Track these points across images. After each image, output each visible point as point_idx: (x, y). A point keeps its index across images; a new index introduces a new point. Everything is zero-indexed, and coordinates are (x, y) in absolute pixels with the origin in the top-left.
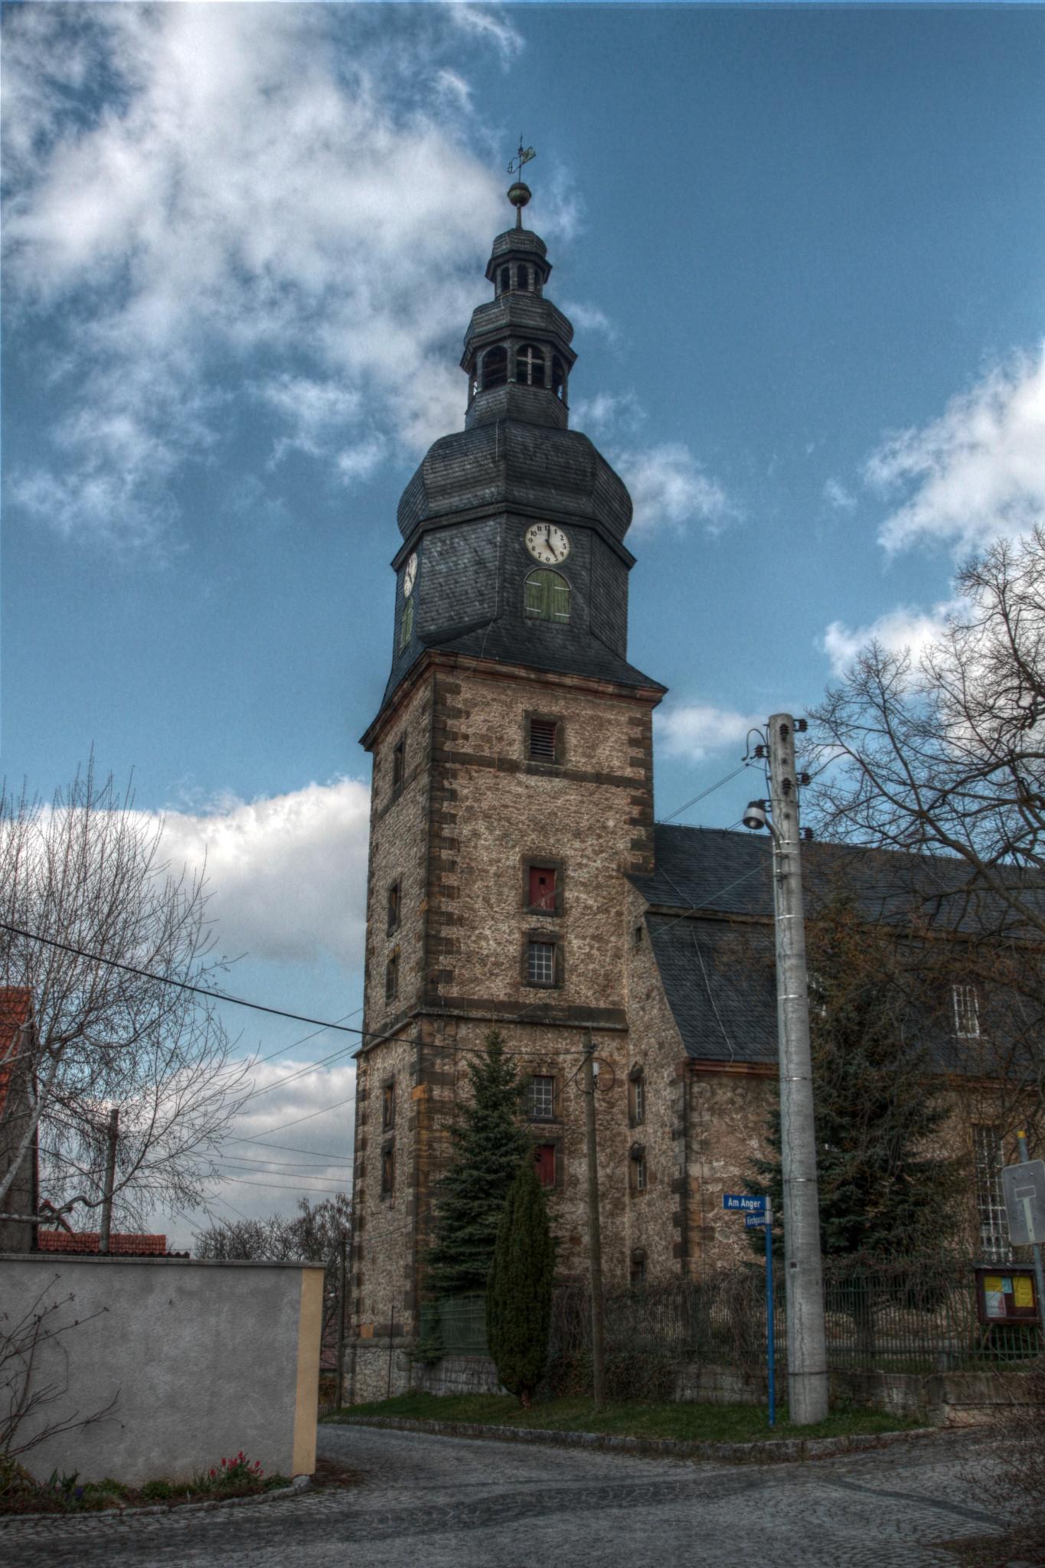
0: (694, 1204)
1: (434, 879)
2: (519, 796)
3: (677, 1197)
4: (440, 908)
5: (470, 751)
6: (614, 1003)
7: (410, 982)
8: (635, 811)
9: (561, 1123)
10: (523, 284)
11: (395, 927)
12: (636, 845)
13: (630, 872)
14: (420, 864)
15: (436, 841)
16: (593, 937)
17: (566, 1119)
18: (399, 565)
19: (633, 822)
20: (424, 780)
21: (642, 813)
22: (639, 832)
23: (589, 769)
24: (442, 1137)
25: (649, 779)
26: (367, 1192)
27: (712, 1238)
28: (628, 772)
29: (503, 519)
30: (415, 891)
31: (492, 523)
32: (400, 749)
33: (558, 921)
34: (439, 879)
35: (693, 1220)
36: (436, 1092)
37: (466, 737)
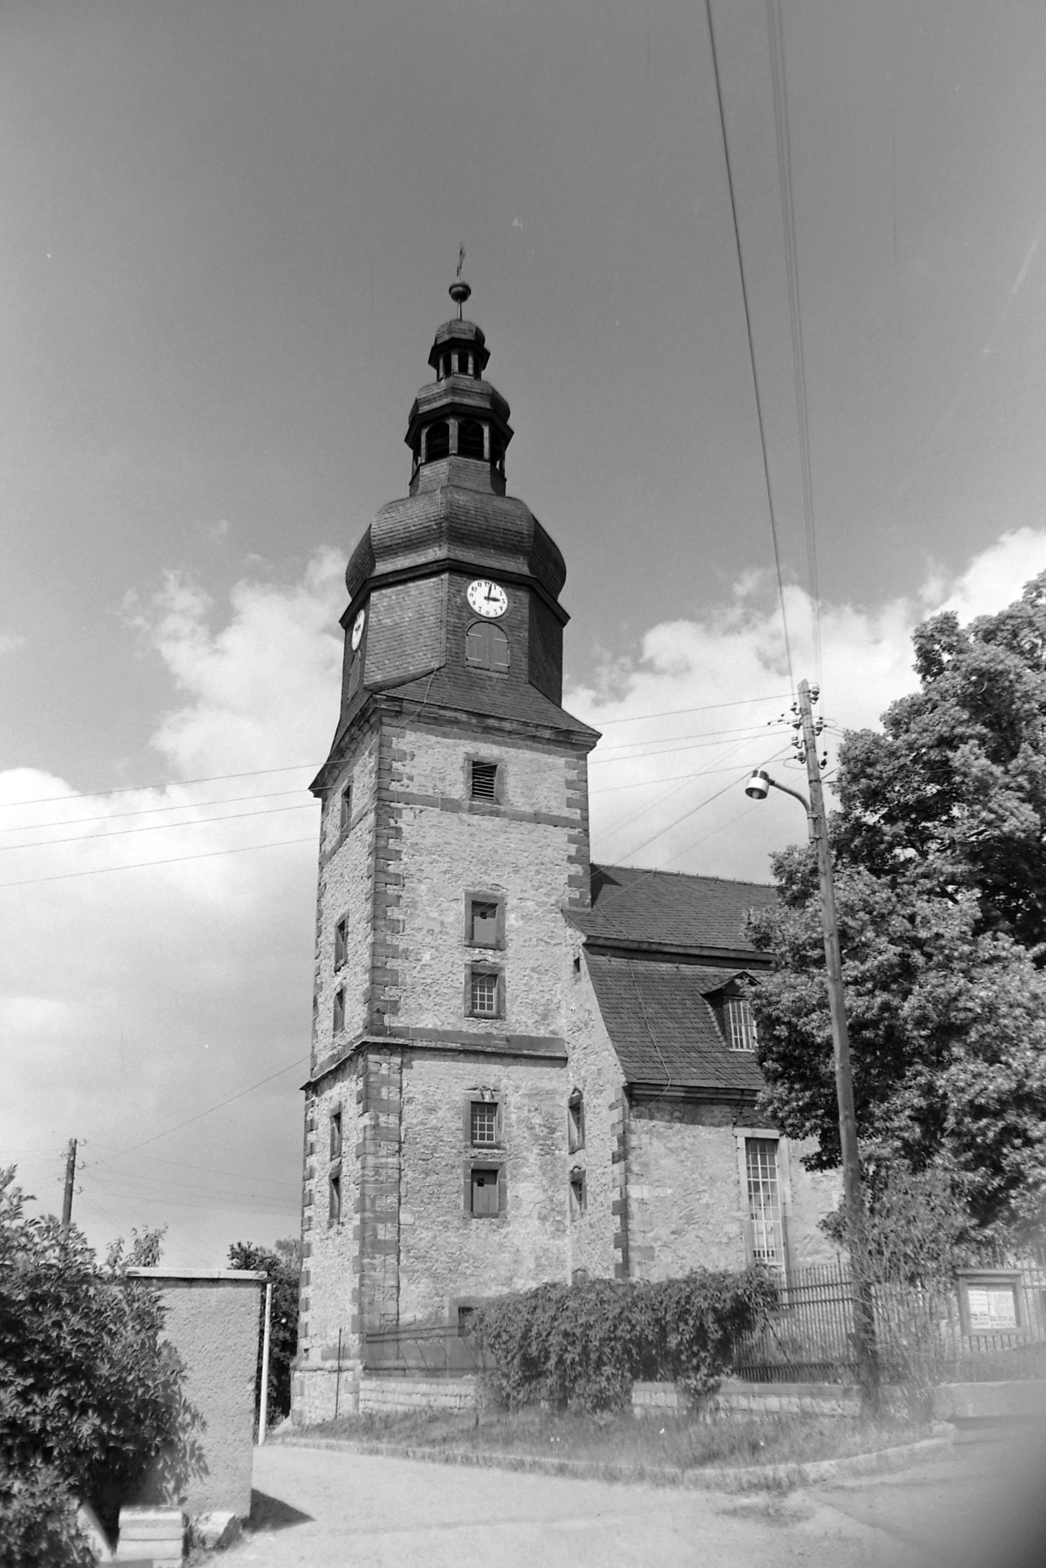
0: (633, 1225)
1: (380, 913)
2: (461, 834)
3: (618, 1218)
4: (385, 940)
5: (415, 791)
6: (553, 1032)
7: (356, 1013)
8: (572, 849)
9: (504, 1149)
10: (463, 369)
11: (342, 962)
12: (572, 881)
13: (568, 907)
14: (367, 900)
15: (382, 877)
16: (533, 970)
17: (508, 1146)
18: (348, 621)
19: (571, 859)
20: (371, 817)
21: (578, 851)
22: (577, 869)
23: (529, 810)
24: (387, 1163)
25: (586, 819)
26: (315, 1219)
27: (652, 1258)
28: (566, 812)
29: (445, 576)
30: (363, 924)
31: (434, 579)
32: (347, 794)
33: (499, 953)
34: (385, 913)
35: (635, 1241)
36: (383, 1119)
37: (411, 778)
